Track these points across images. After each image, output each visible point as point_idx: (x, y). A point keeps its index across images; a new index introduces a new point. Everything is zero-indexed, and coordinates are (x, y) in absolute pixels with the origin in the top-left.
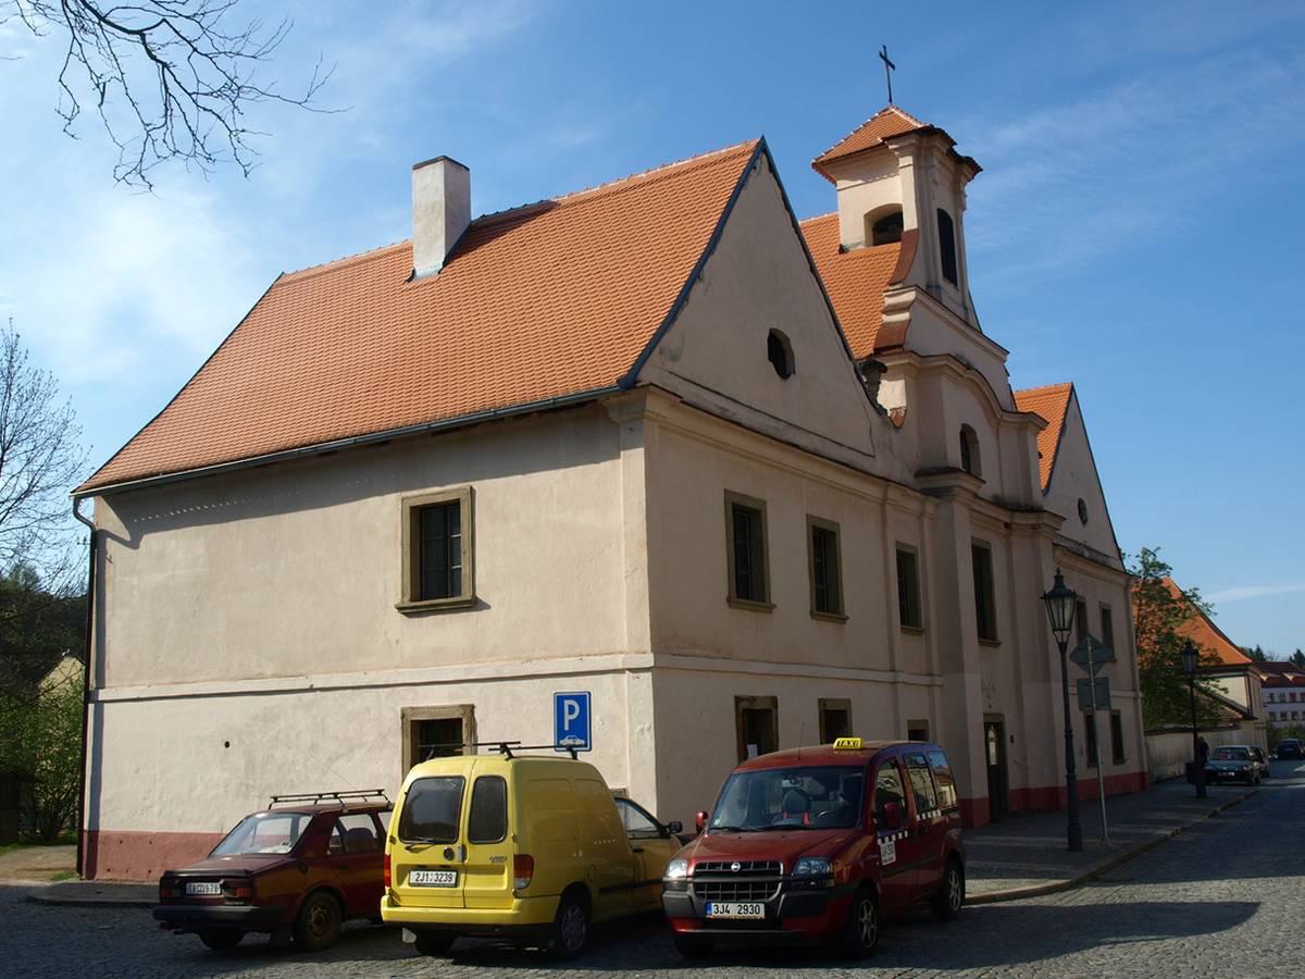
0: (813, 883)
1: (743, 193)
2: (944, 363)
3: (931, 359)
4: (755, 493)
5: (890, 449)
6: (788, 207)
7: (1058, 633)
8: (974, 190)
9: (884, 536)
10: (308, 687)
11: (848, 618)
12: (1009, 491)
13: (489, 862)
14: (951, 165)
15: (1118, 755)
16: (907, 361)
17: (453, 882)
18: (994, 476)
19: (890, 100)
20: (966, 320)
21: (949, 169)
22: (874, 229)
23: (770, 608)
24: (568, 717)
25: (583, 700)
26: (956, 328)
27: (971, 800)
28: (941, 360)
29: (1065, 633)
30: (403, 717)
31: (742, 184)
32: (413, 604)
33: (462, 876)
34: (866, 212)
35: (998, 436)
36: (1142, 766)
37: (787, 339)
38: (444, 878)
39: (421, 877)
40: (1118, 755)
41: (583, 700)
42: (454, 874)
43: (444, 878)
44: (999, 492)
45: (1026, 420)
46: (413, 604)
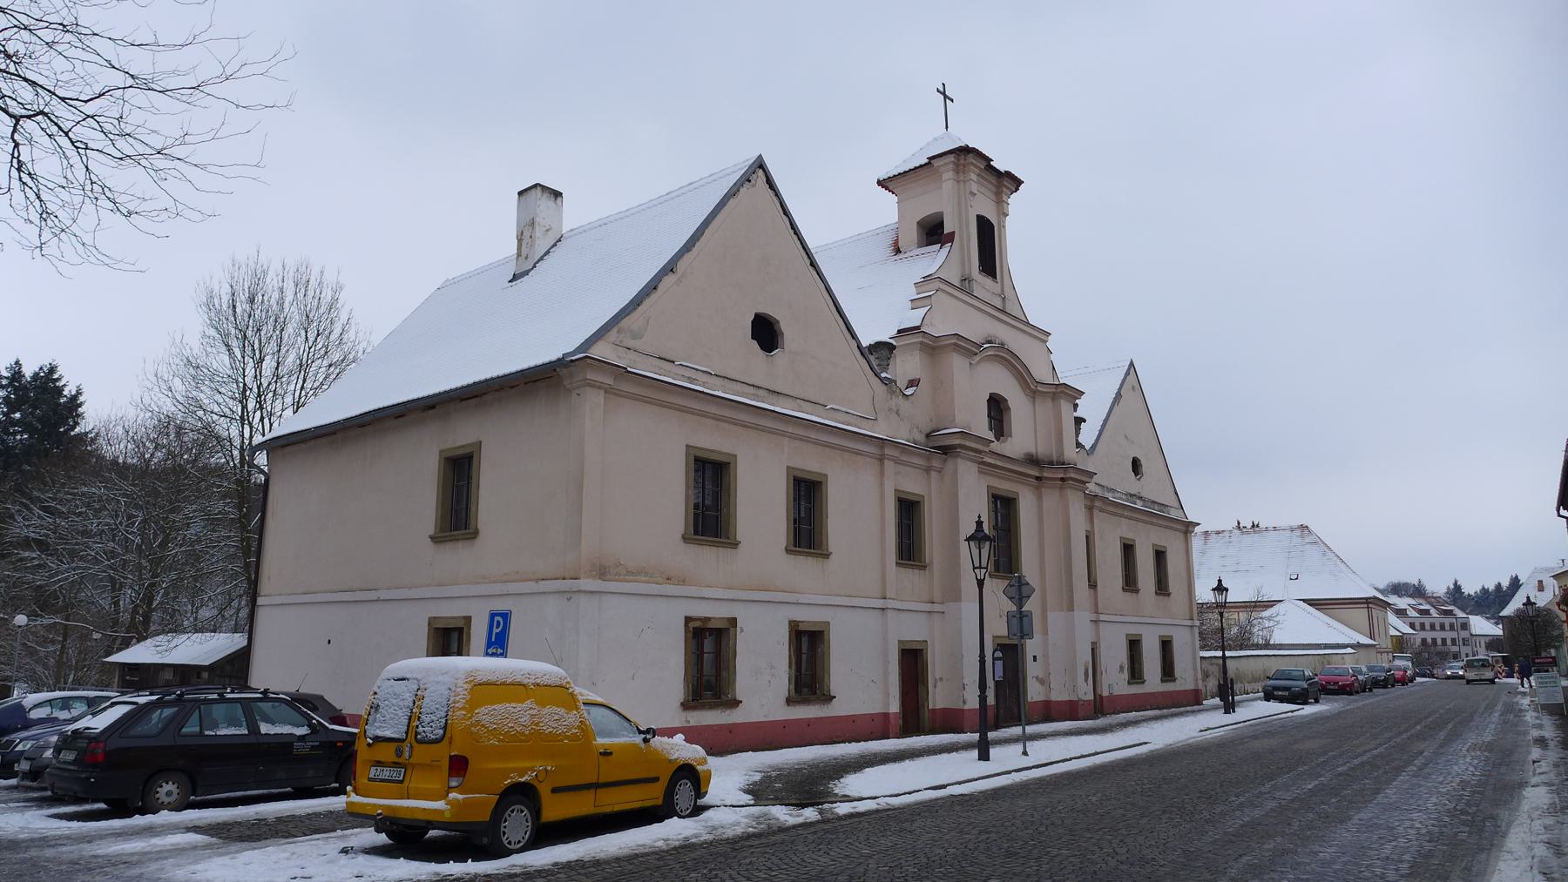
0: (92, 780)
1: (732, 202)
2: (953, 341)
3: (943, 338)
4: (730, 450)
5: (897, 413)
6: (786, 212)
7: (977, 571)
8: (1015, 201)
9: (882, 485)
10: (376, 599)
11: (831, 553)
12: (1042, 449)
13: (429, 762)
14: (993, 179)
15: (1168, 672)
16: (920, 339)
17: (401, 778)
18: (1023, 437)
19: (947, 127)
20: (1007, 312)
21: (991, 183)
22: (927, 234)
23: (735, 545)
24: (496, 630)
25: (506, 616)
26: (994, 317)
27: (889, 713)
28: (951, 339)
29: (983, 571)
30: (429, 624)
31: (733, 193)
32: (443, 534)
33: (409, 772)
34: (918, 219)
35: (1034, 405)
36: (1196, 684)
37: (778, 322)
38: (395, 775)
39: (378, 773)
40: (1168, 672)
41: (506, 616)
42: (403, 770)
43: (395, 775)
44: (1033, 450)
45: (1059, 390)
46: (443, 534)
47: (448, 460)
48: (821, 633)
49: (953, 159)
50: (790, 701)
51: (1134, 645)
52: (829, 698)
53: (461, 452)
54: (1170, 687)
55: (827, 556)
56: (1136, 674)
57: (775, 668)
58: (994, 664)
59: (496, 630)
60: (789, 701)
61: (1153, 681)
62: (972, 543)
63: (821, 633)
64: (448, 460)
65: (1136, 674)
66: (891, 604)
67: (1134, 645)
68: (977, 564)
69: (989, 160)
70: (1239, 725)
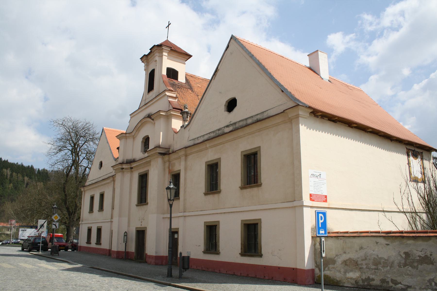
15: (99, 242)
24: (321, 221)
40: (99, 242)
47: (208, 165)
48: (216, 226)
49: (145, 58)
50: (205, 252)
51: (90, 230)
52: (261, 256)
53: (144, 173)
54: (98, 247)
55: (219, 192)
56: (89, 242)
57: (378, 242)
58: (124, 237)
59: (321, 221)
60: (205, 252)
61: (93, 244)
62: (168, 190)
63: (216, 226)
64: (208, 165)
65: (89, 242)
66: (187, 214)
67: (90, 230)
68: (169, 198)
69: (145, 55)
70: (62, 259)
